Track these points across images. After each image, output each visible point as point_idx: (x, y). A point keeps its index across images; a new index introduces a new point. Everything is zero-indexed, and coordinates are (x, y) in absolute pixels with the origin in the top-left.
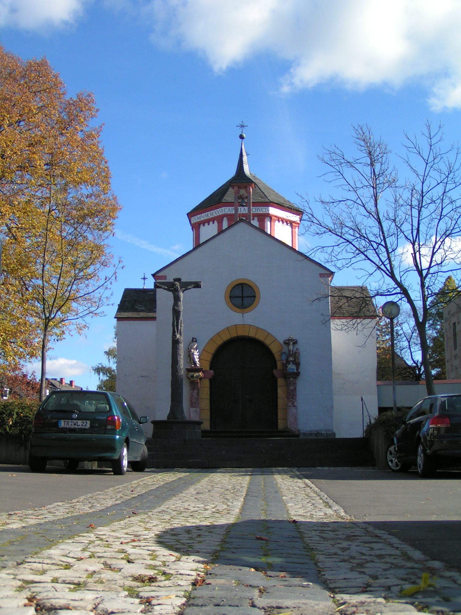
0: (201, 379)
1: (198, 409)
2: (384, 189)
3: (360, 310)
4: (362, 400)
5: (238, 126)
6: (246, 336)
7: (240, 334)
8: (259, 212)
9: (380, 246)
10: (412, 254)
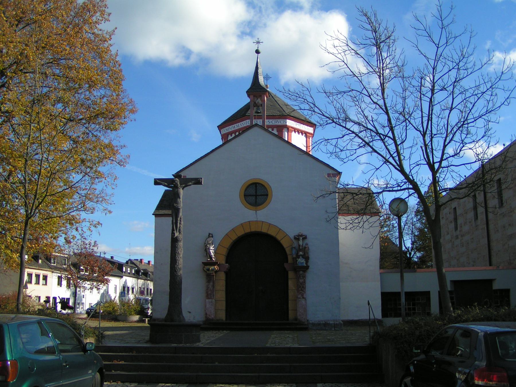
0: (216, 272)
1: (214, 300)
2: (390, 79)
3: (366, 207)
4: (369, 304)
5: (254, 43)
6: (258, 232)
7: (253, 230)
8: (278, 124)
10: (421, 147)
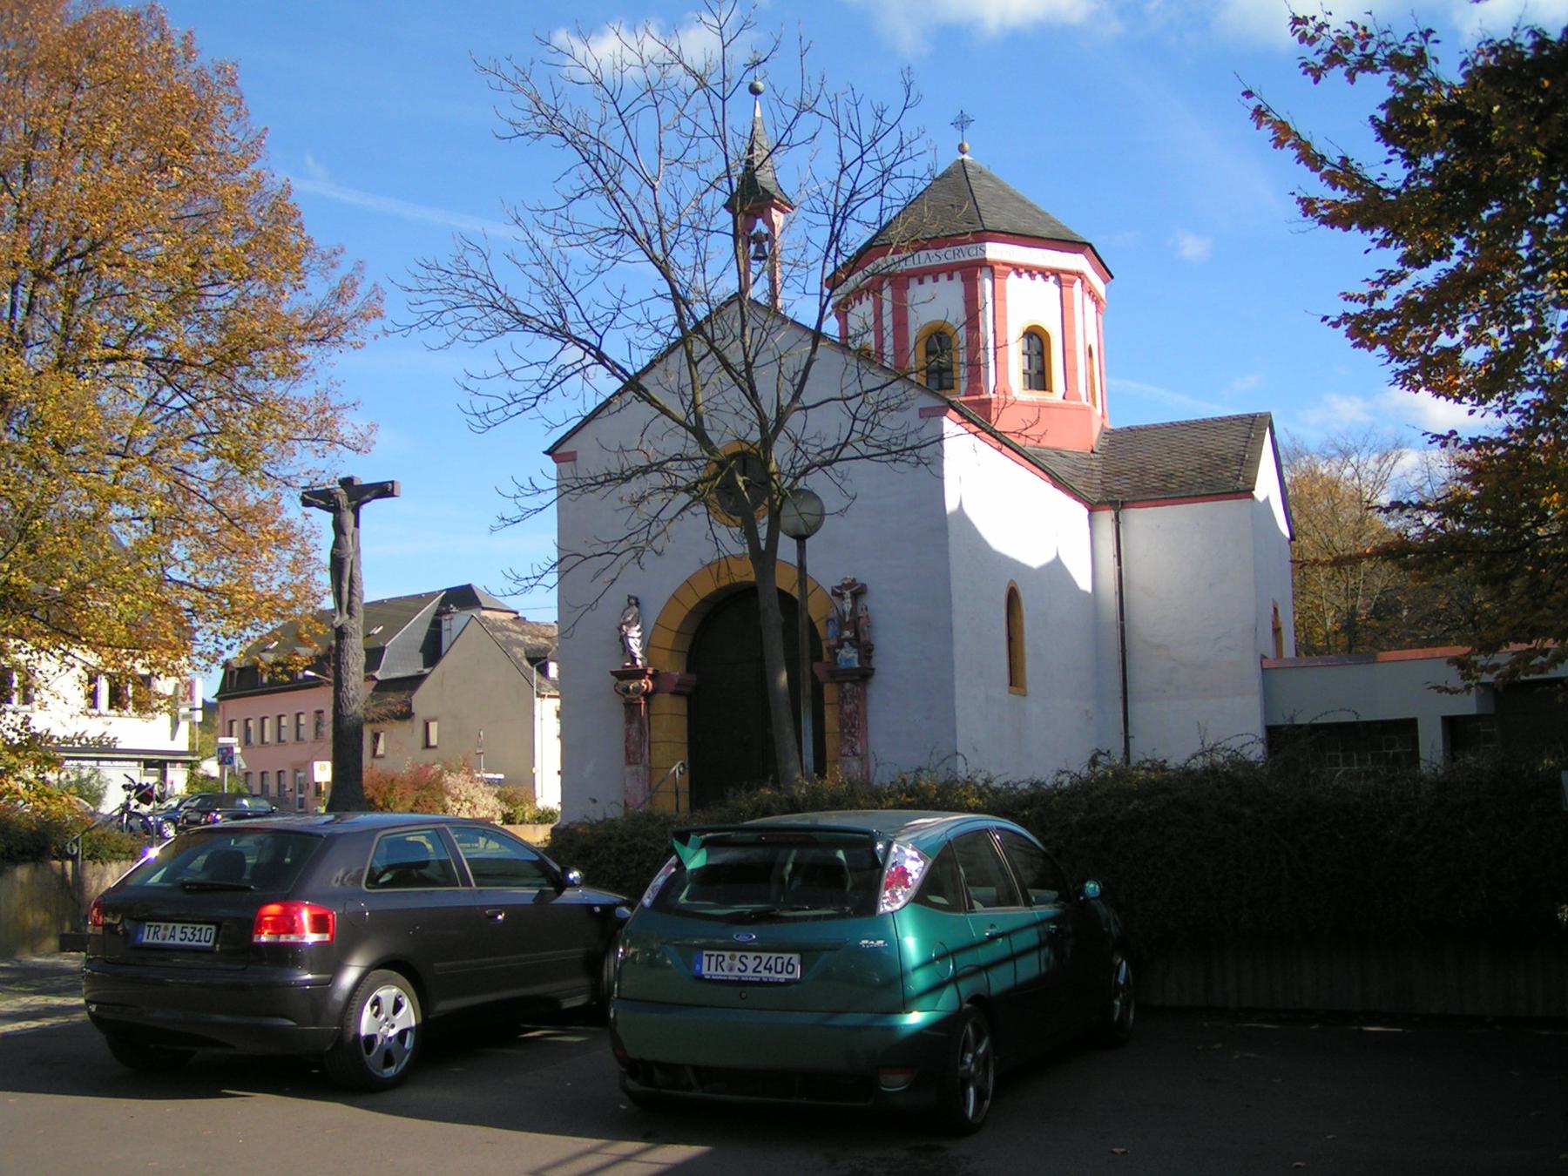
0: (648, 696)
8: (962, 259)
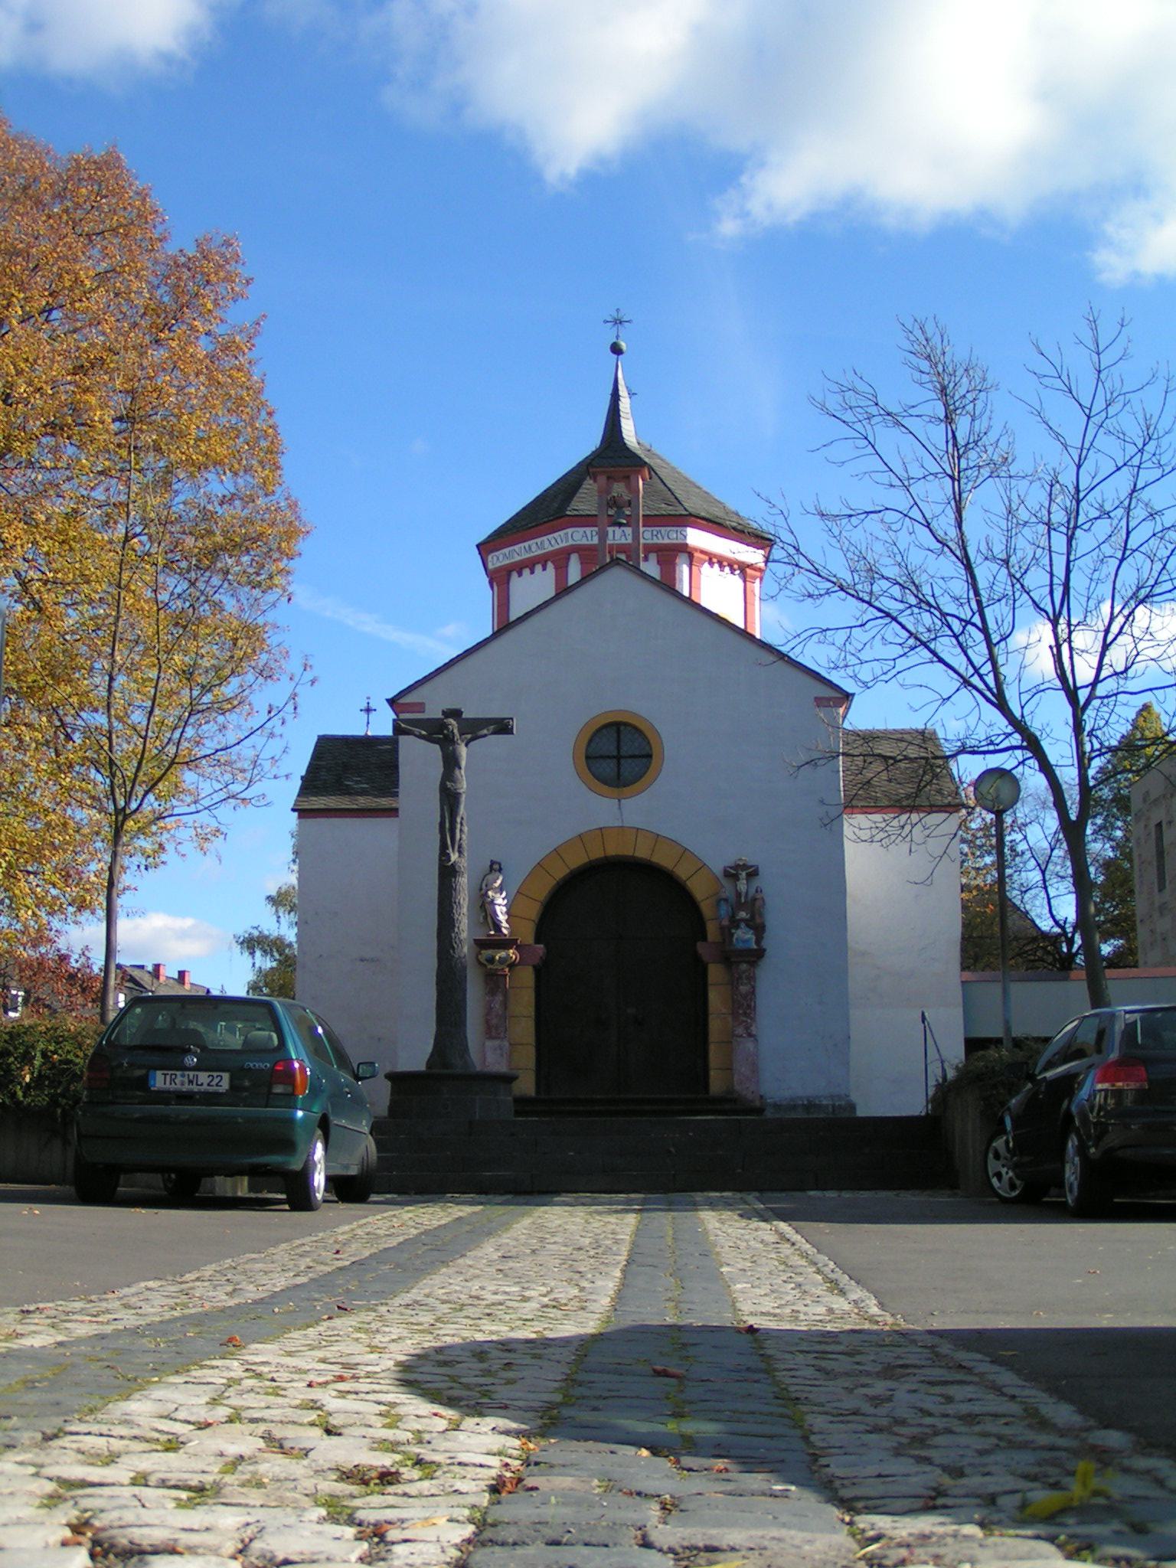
0: (512, 966)
1: (506, 1044)
2: (979, 481)
3: (919, 790)
4: (924, 1019)
5: (606, 322)
6: (627, 856)
7: (612, 851)
8: (660, 541)
9: (969, 627)
10: (1051, 647)
